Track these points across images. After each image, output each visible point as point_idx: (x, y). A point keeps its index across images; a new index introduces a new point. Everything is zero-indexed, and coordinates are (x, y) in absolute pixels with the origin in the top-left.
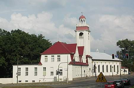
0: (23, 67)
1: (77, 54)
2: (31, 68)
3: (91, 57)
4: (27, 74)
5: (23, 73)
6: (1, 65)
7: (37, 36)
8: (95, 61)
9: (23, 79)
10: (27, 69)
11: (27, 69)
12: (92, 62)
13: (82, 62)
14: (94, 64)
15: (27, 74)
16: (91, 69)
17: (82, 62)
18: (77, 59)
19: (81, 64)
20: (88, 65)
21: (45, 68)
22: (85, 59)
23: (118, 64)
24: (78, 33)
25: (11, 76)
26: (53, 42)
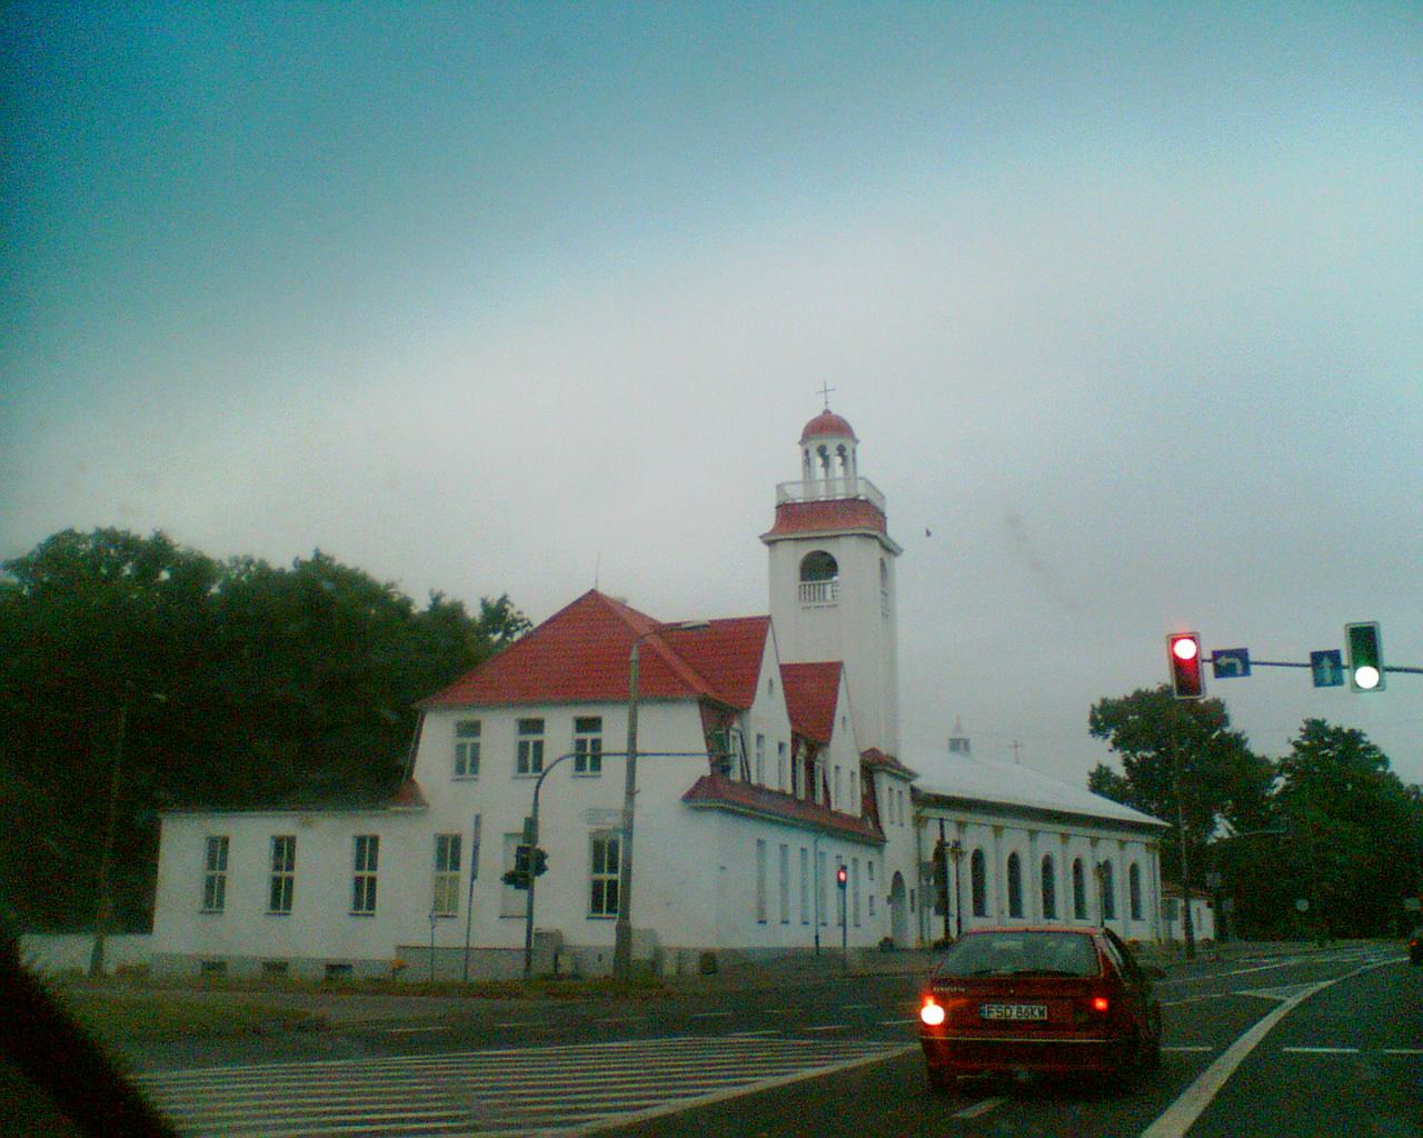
0: (251, 837)
1: (769, 716)
2: (325, 844)
3: (906, 776)
4: (281, 896)
5: (238, 892)
6: (1421, 961)
7: (474, 612)
8: (942, 813)
9: (246, 932)
10: (284, 850)
11: (284, 850)
12: (919, 822)
13: (820, 800)
14: (931, 835)
15: (281, 896)
16: (910, 881)
17: (820, 800)
18: (772, 768)
19: (806, 809)
20: (876, 840)
21: (448, 851)
22: (858, 787)
23: (1140, 855)
24: (794, 554)
25: (138, 918)
26: (716, 812)
